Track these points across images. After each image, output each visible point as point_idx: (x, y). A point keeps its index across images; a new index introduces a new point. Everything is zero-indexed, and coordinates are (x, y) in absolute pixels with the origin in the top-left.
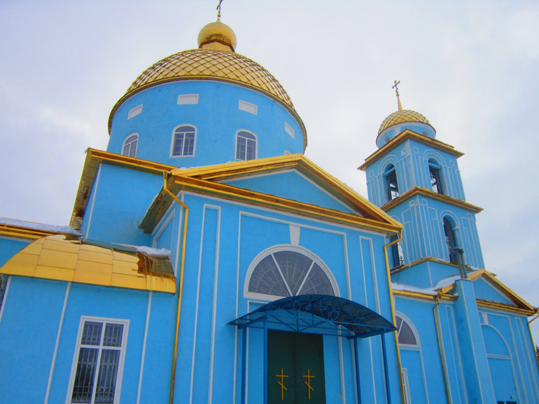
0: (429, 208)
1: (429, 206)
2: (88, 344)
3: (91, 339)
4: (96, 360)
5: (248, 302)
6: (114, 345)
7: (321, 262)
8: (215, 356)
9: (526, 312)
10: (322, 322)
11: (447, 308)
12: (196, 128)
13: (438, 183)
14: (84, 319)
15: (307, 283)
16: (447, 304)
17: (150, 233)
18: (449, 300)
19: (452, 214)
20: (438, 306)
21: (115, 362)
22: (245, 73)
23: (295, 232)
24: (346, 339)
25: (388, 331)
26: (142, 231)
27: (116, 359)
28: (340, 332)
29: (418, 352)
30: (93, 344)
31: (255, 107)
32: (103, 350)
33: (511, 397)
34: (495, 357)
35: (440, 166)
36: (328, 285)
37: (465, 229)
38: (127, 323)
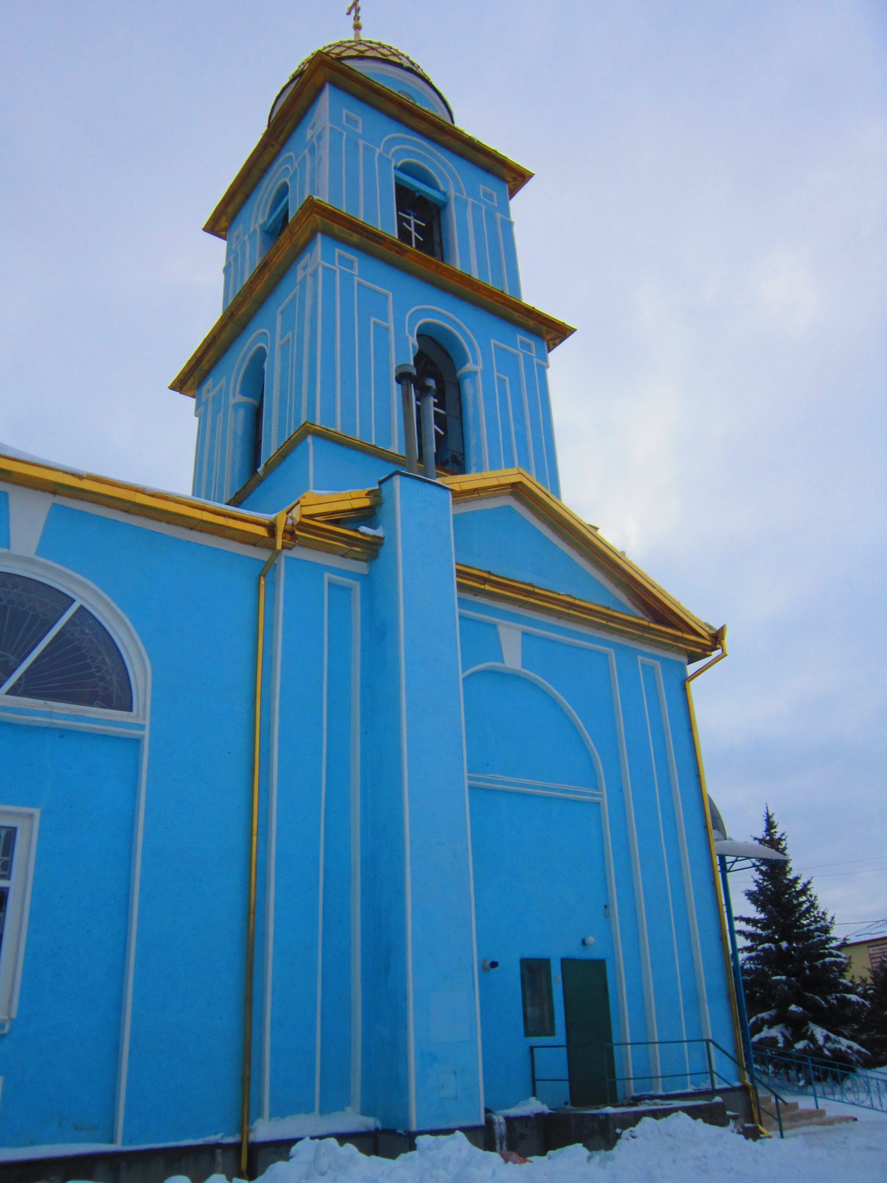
0: (359, 284)
1: (360, 276)
16: (331, 570)
29: (137, 742)
33: (584, 943)
34: (510, 784)
35: (445, 194)
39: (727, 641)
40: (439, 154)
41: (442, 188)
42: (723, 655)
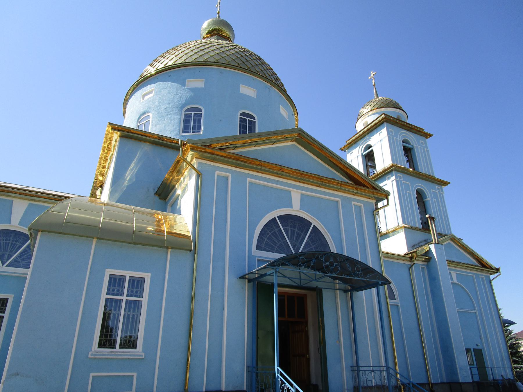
2: (113, 294)
3: (116, 290)
4: (120, 310)
5: (257, 259)
6: (136, 296)
7: (319, 223)
8: (228, 307)
9: (489, 271)
10: (322, 277)
11: (421, 267)
12: (203, 109)
13: (410, 160)
14: (109, 272)
15: (307, 243)
17: (165, 200)
18: (423, 261)
19: (423, 187)
20: (413, 266)
21: (138, 311)
22: (244, 61)
23: (296, 196)
24: (342, 292)
25: (383, 284)
26: (157, 198)
27: (138, 309)
28: (337, 286)
29: (398, 306)
30: (117, 295)
31: (255, 91)
32: (127, 300)
36: (326, 245)
37: (435, 201)
38: (148, 276)
39: (501, 270)
40: (409, 134)
41: (412, 144)
42: (500, 274)
